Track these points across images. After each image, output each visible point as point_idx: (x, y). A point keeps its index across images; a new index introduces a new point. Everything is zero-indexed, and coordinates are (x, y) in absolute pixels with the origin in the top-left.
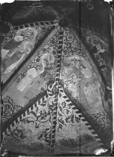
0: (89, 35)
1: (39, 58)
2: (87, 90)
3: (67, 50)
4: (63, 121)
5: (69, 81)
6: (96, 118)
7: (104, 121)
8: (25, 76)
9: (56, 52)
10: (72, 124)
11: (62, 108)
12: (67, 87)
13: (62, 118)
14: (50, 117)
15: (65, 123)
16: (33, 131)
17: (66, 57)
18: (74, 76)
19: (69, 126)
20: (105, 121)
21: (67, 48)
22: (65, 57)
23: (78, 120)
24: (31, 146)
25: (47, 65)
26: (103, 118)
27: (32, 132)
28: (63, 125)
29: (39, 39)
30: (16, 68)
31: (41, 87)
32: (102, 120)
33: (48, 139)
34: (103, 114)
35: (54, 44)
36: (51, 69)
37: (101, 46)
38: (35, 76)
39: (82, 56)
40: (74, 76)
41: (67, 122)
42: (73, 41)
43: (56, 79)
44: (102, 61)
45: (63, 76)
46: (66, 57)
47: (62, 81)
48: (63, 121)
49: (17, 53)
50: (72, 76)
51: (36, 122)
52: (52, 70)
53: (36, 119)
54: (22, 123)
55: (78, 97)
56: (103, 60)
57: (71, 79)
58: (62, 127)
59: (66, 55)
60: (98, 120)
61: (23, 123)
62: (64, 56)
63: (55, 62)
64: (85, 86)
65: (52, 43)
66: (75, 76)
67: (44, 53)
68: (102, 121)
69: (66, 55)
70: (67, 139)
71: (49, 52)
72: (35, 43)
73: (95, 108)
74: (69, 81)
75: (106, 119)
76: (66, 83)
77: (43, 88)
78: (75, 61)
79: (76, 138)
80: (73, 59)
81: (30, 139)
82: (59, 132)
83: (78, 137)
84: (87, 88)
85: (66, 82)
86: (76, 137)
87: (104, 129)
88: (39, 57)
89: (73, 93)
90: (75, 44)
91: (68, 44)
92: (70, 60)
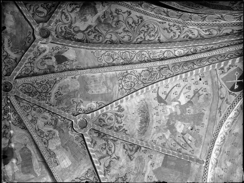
0: (32, 68)
1: (40, 131)
2: (92, 91)
3: (42, 96)
4: (119, 126)
5: (77, 106)
6: (123, 89)
7: (128, 82)
8: (55, 154)
9: (39, 109)
10: (124, 117)
11: (105, 124)
12: (83, 110)
13: (116, 127)
14: (111, 139)
15: (122, 125)
16: (121, 164)
17: (49, 101)
18: (73, 100)
19: (126, 122)
20: (128, 80)
21: (40, 96)
22: (49, 102)
23: (122, 110)
24: (137, 171)
25: (51, 125)
26: (124, 81)
27: (122, 166)
28: (123, 128)
29: (17, 122)
30: (39, 160)
31: (75, 140)
32: (126, 83)
33: (134, 148)
34: (121, 81)
35: (29, 108)
36: (57, 121)
37: (48, 58)
38: (60, 143)
39: (54, 84)
40: (73, 100)
41: (122, 122)
42: (34, 87)
43: (30, 49)
44: (65, 65)
45: (69, 111)
46: (49, 101)
47: (74, 113)
48: (119, 126)
49: (22, 153)
50: (72, 102)
51: (113, 157)
52: (58, 120)
53: (109, 157)
54: (109, 175)
55: (97, 102)
56: (64, 62)
57: (75, 104)
58: (126, 129)
59: (48, 100)
60: (125, 88)
61: (108, 173)
62: (48, 102)
63: (50, 114)
64: (88, 91)
65: (28, 110)
66: (73, 99)
67: (36, 123)
68: (127, 83)
69: (48, 100)
70: (140, 127)
71: (38, 118)
72: (20, 128)
73: (113, 88)
74: (77, 106)
75: (126, 79)
76: (78, 110)
77: (76, 138)
78: (58, 94)
79: (140, 116)
80: (55, 95)
81: (129, 170)
82: (130, 134)
83: (139, 114)
84: (90, 90)
85: (76, 110)
86: (140, 116)
87: (136, 83)
88: (39, 130)
89: (91, 107)
90: (39, 86)
91: (36, 93)
92: (55, 98)
